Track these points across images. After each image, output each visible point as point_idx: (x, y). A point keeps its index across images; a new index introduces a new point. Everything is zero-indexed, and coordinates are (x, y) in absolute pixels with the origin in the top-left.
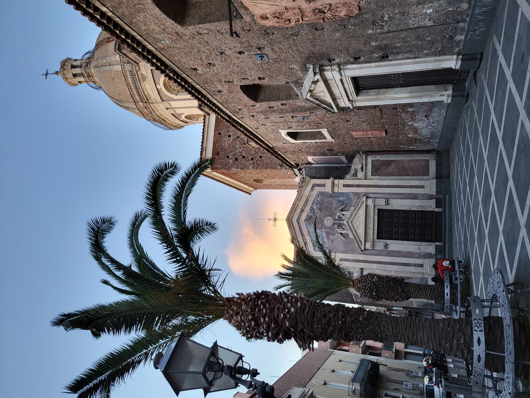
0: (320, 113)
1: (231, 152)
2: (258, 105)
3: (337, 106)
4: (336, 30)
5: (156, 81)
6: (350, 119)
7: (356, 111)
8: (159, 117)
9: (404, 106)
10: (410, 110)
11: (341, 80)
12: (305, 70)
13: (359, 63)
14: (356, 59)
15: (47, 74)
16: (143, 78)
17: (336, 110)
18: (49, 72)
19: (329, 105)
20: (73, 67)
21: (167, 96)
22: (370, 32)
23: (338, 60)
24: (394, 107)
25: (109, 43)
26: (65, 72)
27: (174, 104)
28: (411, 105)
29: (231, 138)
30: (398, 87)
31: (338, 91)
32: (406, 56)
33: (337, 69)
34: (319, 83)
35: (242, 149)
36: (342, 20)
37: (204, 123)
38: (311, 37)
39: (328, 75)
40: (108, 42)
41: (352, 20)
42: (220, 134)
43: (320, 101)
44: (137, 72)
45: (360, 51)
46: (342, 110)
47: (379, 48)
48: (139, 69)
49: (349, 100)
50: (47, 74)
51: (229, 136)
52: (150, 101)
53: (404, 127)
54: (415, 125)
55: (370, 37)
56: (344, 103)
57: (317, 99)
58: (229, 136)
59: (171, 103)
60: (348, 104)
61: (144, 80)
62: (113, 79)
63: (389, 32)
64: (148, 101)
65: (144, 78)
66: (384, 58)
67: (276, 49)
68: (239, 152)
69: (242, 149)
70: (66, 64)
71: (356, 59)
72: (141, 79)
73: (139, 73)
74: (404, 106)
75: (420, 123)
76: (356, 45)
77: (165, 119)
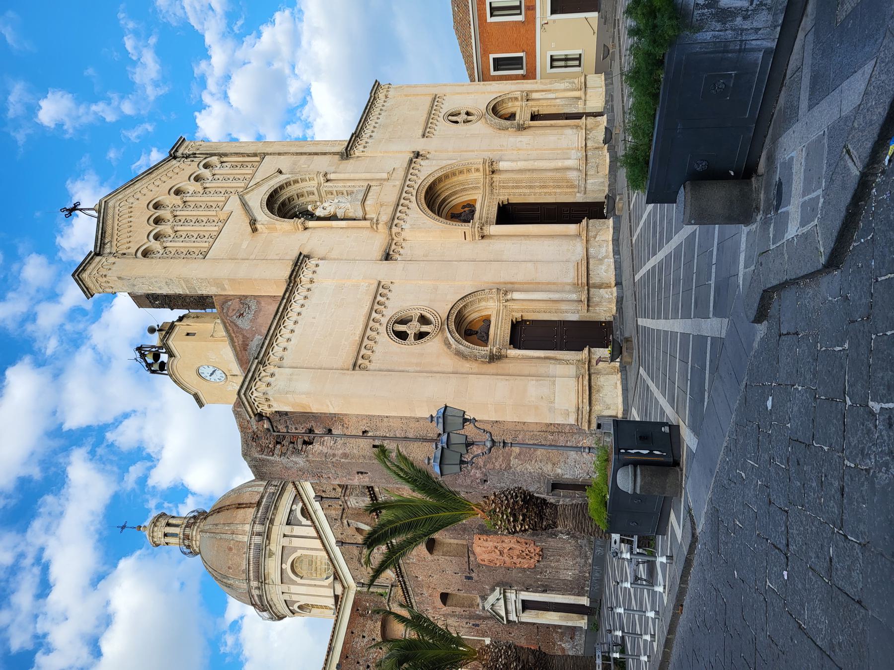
0: (491, 623)
1: (363, 656)
2: (445, 608)
3: (507, 618)
4: (519, 572)
5: (284, 559)
6: (513, 632)
7: (519, 625)
8: (268, 602)
9: (556, 627)
10: (559, 630)
11: (515, 601)
12: (493, 590)
13: (529, 591)
14: (527, 589)
15: (123, 527)
16: (269, 553)
17: (505, 622)
18: (127, 525)
19: (502, 618)
20: (168, 525)
21: (290, 577)
22: (539, 577)
23: (516, 588)
24: (548, 626)
25: (239, 509)
26: (156, 529)
27: (294, 589)
28: (560, 627)
29: (366, 640)
30: (551, 611)
31: (511, 607)
32: (558, 593)
33: (515, 593)
34: (500, 600)
35: (376, 654)
36: (524, 568)
37: (337, 617)
38: (504, 572)
39: (508, 594)
40: (238, 508)
41: (530, 570)
42: (352, 633)
43: (496, 613)
44: (265, 547)
45: (531, 585)
46: (509, 621)
47: (542, 585)
48: (269, 543)
49: (517, 616)
50: (123, 527)
51: (364, 637)
52: (267, 581)
53: (554, 646)
54: (563, 645)
55: (538, 580)
56: (513, 617)
57: (494, 611)
58: (364, 637)
59: (292, 587)
60: (515, 619)
61: (270, 556)
62: (230, 549)
63: (549, 578)
64: (265, 580)
65: (271, 554)
66: (544, 591)
67: (480, 575)
68: (373, 658)
69: (376, 654)
70: (160, 519)
71: (527, 589)
72: (267, 556)
73: (268, 548)
74: (555, 626)
75: (567, 644)
76: (529, 582)
77: (273, 605)
